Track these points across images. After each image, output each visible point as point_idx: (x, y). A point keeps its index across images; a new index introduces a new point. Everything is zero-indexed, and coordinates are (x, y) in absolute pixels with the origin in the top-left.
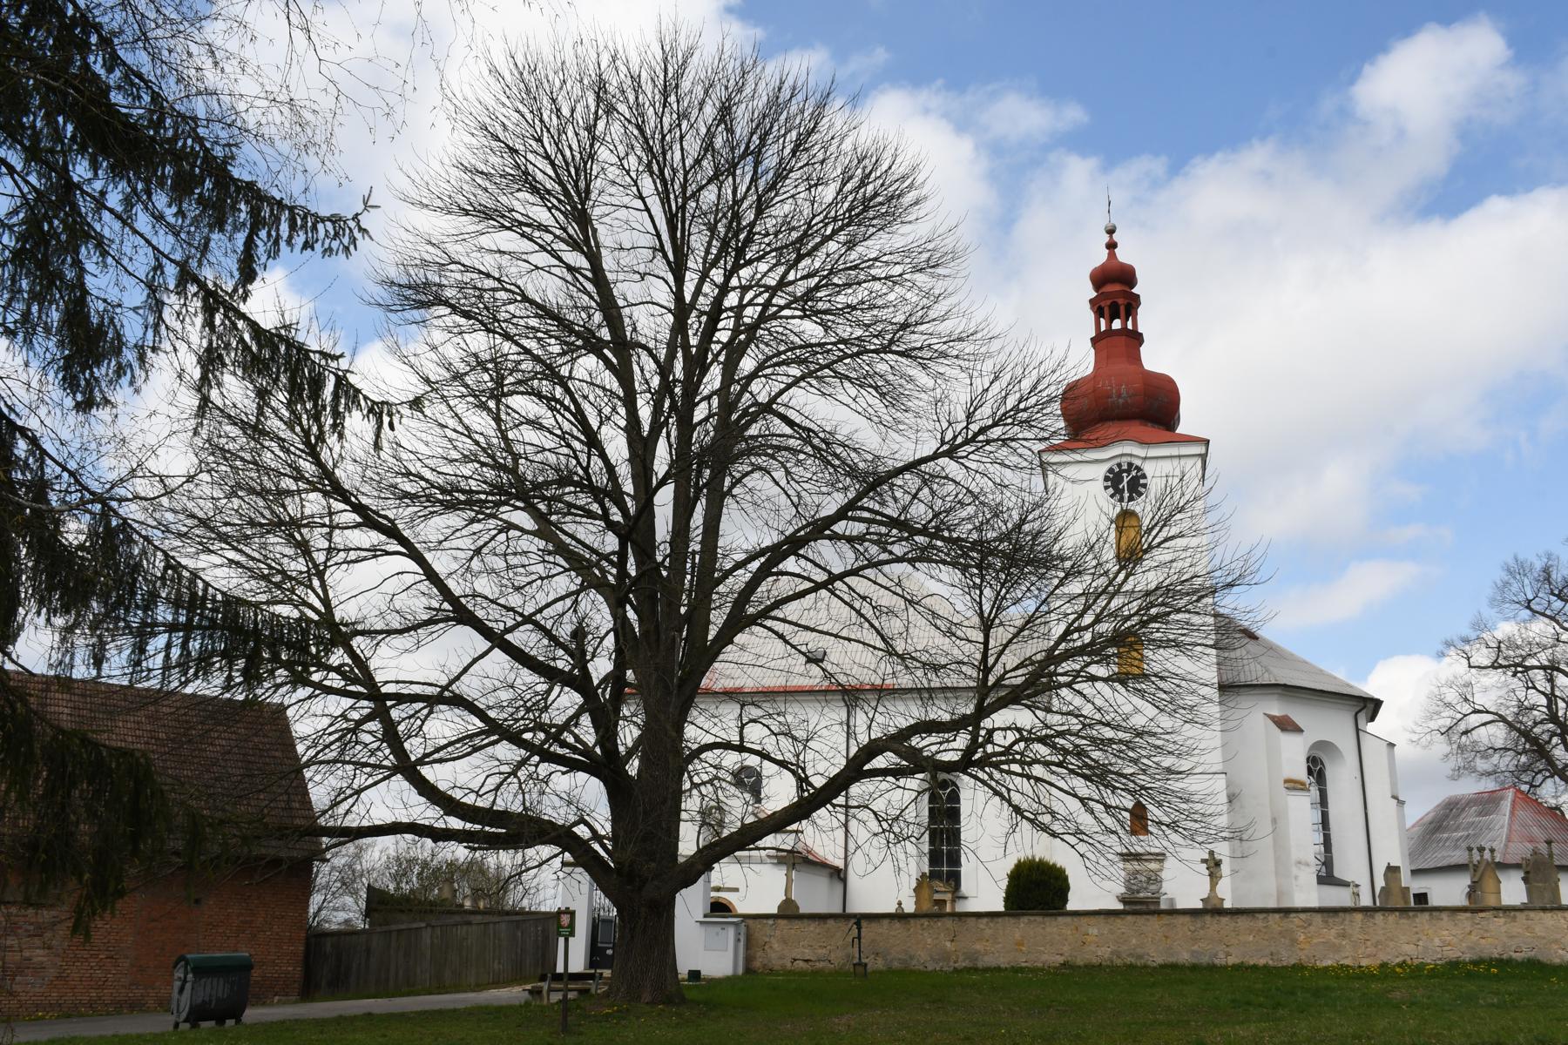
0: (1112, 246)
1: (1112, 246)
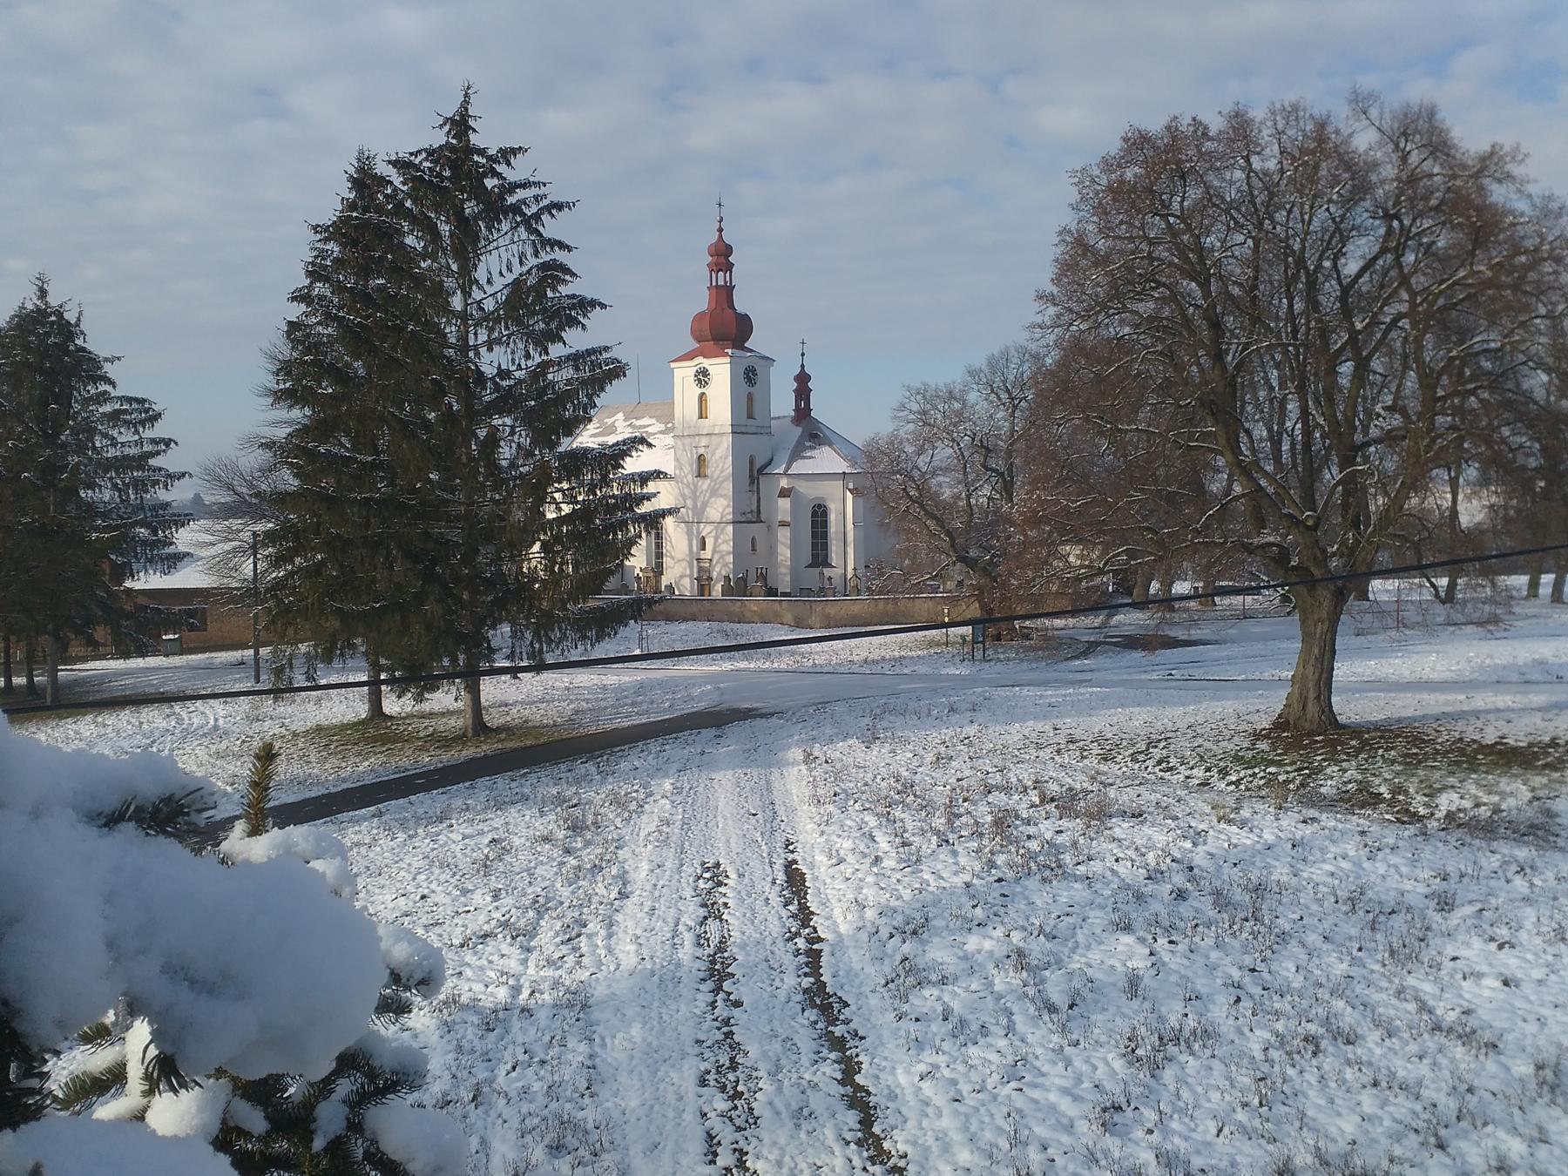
0: (720, 230)
1: (720, 230)
